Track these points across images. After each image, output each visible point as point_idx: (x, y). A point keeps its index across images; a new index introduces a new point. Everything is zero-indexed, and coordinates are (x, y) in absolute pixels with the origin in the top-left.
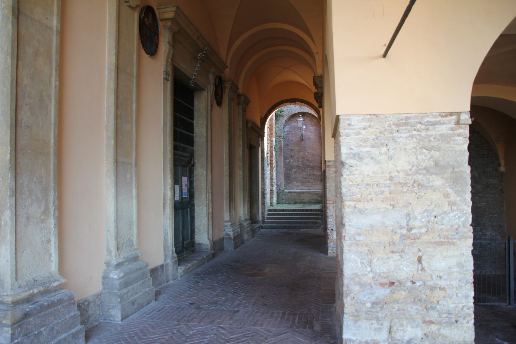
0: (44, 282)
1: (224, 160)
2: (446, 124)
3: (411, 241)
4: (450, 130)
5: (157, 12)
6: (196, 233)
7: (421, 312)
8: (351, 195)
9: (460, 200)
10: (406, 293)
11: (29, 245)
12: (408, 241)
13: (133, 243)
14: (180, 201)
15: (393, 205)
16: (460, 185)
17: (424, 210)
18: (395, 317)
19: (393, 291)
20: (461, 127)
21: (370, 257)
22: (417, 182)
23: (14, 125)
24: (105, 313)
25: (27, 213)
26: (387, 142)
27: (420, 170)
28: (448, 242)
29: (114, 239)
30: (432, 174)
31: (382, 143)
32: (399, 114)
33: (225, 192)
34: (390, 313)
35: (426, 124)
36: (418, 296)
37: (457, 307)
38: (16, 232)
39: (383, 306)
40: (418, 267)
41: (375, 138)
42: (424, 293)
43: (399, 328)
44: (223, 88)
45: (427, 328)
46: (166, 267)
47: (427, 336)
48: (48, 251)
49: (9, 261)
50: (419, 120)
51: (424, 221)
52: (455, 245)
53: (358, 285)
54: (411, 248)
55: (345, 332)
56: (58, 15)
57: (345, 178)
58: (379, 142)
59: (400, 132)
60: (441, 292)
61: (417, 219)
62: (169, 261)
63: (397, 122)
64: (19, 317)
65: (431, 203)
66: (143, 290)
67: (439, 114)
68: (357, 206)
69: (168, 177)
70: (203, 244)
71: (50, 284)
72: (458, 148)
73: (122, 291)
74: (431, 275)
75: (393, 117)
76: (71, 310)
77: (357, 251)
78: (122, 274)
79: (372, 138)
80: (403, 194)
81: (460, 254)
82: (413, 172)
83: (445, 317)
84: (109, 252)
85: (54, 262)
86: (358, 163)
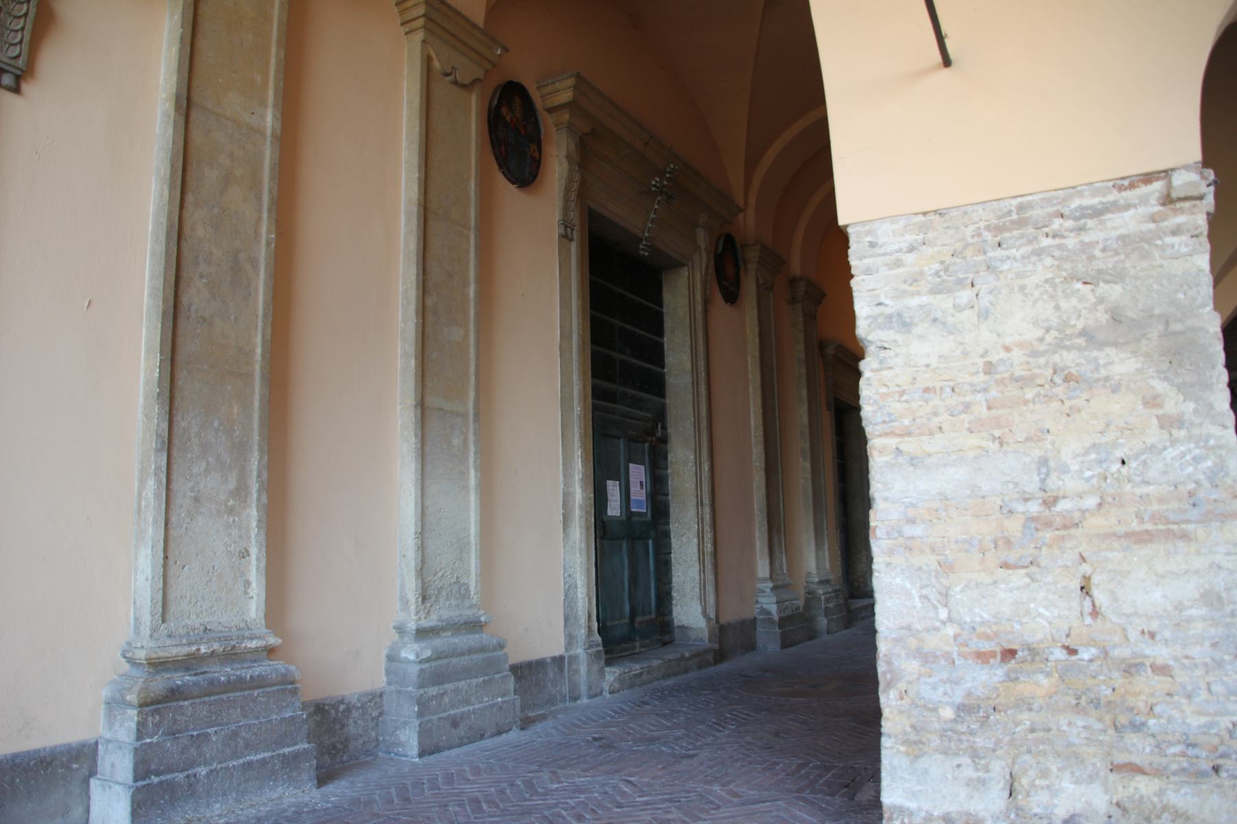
0: (227, 637)
1: (753, 432)
2: (1135, 206)
3: (1057, 532)
4: (1146, 222)
5: (535, 96)
6: (674, 602)
7: (1100, 738)
8: (887, 420)
9: (1196, 411)
10: (1053, 680)
11: (197, 555)
12: (1048, 535)
13: (470, 591)
14: (624, 518)
15: (999, 437)
16: (1191, 368)
17: (1088, 445)
18: (1025, 748)
19: (1013, 675)
20: (1181, 208)
21: (945, 582)
22: (1063, 371)
23: (171, 314)
24: (387, 738)
25: (196, 489)
26: (971, 276)
27: (1069, 337)
28: (1169, 531)
29: (413, 573)
30: (1102, 345)
31: (958, 278)
32: (999, 200)
33: (756, 508)
34: (1008, 738)
35: (1077, 214)
36: (1089, 690)
37: (1211, 725)
38: (166, 524)
39: (988, 717)
40: (1082, 606)
41: (940, 270)
42: (1104, 682)
43: (1037, 782)
44: (741, 264)
45: (1124, 787)
46: (570, 664)
47: (1125, 810)
48: (243, 574)
49: (150, 578)
50: (1055, 209)
51: (1093, 477)
52: (1191, 539)
53: (915, 657)
54: (1056, 551)
55: (887, 786)
56: (275, 106)
57: (868, 379)
58: (951, 278)
59: (1004, 246)
60: (1156, 678)
61: (1068, 472)
62: (580, 651)
63: (996, 222)
64: (157, 692)
65: (1108, 425)
66: (487, 699)
67: (1111, 184)
68: (902, 447)
69: (576, 455)
70: (691, 628)
71: (239, 641)
72: (1177, 267)
73: (426, 690)
74: (1124, 630)
75: (984, 209)
76: (284, 704)
77: (908, 567)
78: (427, 653)
79: (933, 271)
80: (1024, 408)
81: (1210, 567)
82: (1050, 344)
83: (1175, 755)
84: (405, 603)
85: (255, 599)
86: (899, 338)
